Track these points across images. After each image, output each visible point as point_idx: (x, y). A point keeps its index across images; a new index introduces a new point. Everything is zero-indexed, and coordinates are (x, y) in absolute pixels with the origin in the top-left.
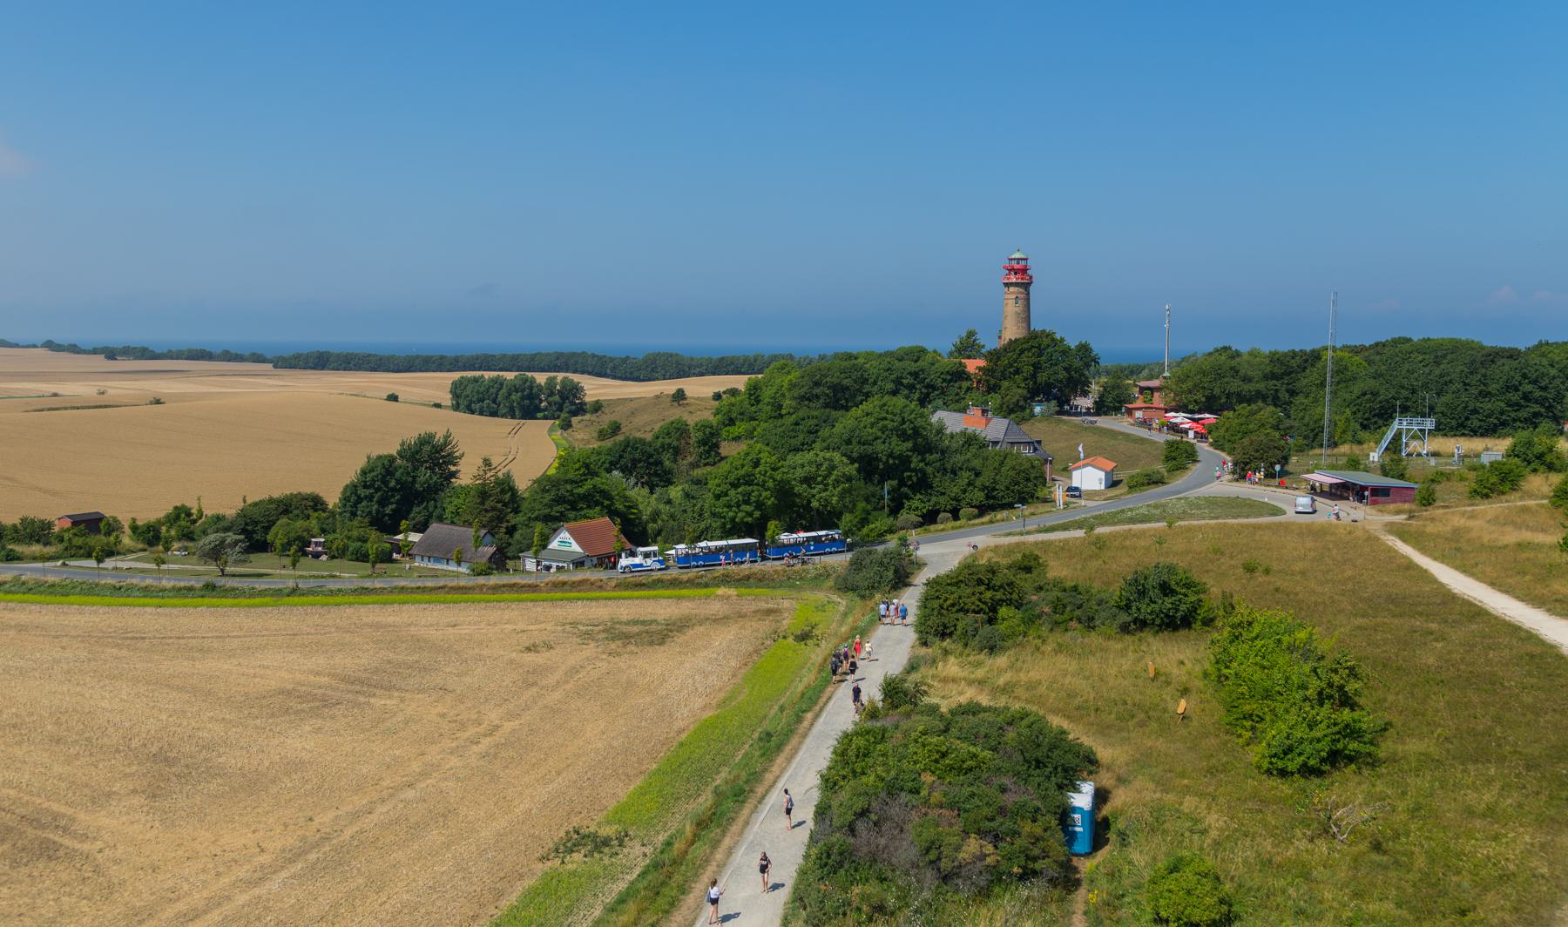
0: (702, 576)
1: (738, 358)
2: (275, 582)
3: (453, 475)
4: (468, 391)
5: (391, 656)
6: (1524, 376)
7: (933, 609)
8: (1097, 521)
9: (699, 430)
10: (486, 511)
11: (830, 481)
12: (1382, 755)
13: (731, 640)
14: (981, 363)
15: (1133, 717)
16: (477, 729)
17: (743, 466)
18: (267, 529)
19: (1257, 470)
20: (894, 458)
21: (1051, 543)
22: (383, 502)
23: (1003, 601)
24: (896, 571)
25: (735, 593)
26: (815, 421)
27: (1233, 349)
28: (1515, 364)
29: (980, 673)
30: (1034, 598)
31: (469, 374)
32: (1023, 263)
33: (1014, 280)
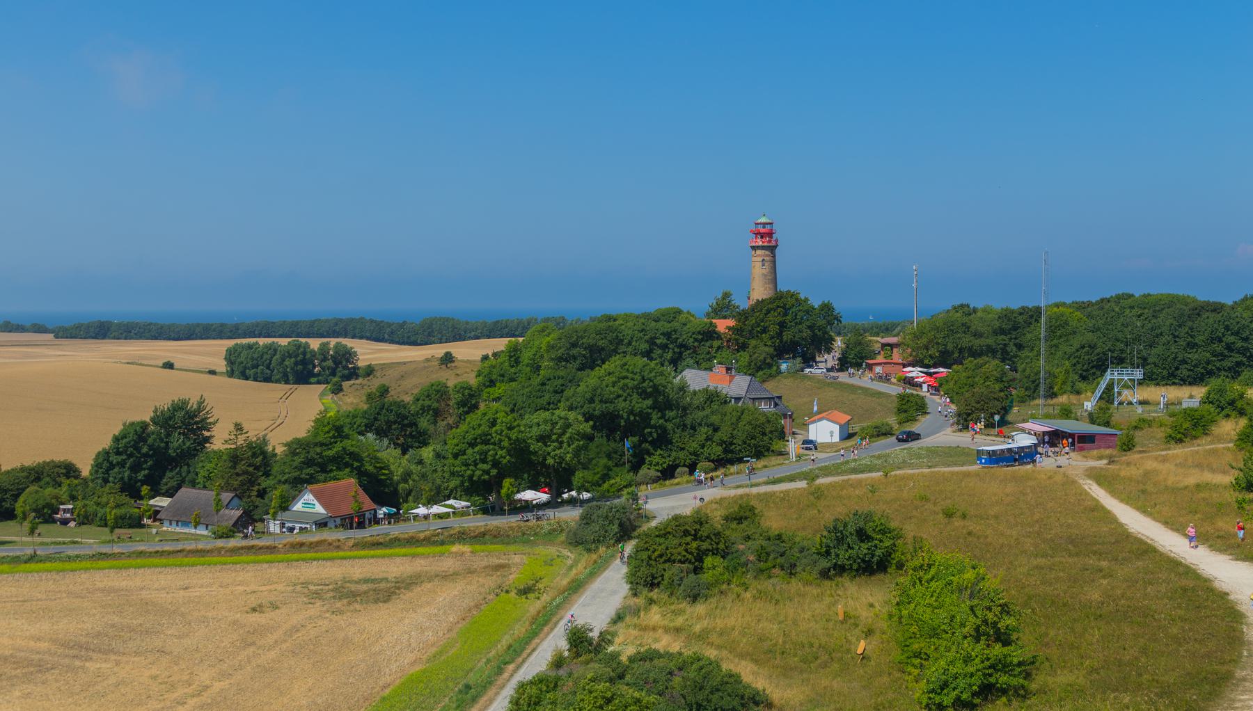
0: (439, 534)
1: (512, 322)
2: (13, 550)
3: (207, 440)
4: (242, 358)
5: (116, 619)
6: (1227, 328)
7: (642, 560)
8: (822, 472)
9: (458, 392)
10: (238, 475)
11: (565, 438)
12: (1033, 686)
13: (455, 596)
14: (731, 323)
15: (816, 658)
16: (186, 690)
17: (480, 425)
18: (16, 497)
19: (978, 420)
20: (635, 415)
21: (772, 494)
22: (136, 468)
23: (708, 550)
24: (621, 525)
25: (468, 550)
26: (561, 381)
27: (971, 306)
28: (1218, 317)
29: (680, 621)
30: (741, 547)
31: (245, 341)
32: (768, 227)
33: (761, 243)
